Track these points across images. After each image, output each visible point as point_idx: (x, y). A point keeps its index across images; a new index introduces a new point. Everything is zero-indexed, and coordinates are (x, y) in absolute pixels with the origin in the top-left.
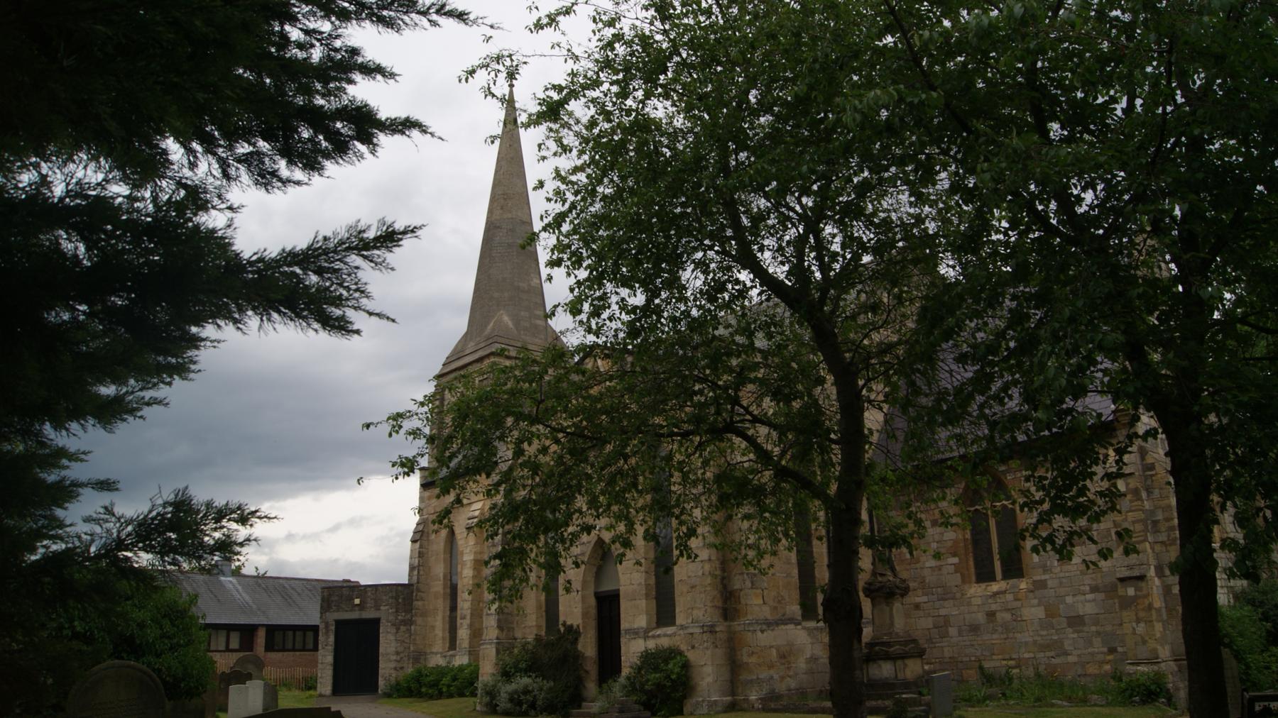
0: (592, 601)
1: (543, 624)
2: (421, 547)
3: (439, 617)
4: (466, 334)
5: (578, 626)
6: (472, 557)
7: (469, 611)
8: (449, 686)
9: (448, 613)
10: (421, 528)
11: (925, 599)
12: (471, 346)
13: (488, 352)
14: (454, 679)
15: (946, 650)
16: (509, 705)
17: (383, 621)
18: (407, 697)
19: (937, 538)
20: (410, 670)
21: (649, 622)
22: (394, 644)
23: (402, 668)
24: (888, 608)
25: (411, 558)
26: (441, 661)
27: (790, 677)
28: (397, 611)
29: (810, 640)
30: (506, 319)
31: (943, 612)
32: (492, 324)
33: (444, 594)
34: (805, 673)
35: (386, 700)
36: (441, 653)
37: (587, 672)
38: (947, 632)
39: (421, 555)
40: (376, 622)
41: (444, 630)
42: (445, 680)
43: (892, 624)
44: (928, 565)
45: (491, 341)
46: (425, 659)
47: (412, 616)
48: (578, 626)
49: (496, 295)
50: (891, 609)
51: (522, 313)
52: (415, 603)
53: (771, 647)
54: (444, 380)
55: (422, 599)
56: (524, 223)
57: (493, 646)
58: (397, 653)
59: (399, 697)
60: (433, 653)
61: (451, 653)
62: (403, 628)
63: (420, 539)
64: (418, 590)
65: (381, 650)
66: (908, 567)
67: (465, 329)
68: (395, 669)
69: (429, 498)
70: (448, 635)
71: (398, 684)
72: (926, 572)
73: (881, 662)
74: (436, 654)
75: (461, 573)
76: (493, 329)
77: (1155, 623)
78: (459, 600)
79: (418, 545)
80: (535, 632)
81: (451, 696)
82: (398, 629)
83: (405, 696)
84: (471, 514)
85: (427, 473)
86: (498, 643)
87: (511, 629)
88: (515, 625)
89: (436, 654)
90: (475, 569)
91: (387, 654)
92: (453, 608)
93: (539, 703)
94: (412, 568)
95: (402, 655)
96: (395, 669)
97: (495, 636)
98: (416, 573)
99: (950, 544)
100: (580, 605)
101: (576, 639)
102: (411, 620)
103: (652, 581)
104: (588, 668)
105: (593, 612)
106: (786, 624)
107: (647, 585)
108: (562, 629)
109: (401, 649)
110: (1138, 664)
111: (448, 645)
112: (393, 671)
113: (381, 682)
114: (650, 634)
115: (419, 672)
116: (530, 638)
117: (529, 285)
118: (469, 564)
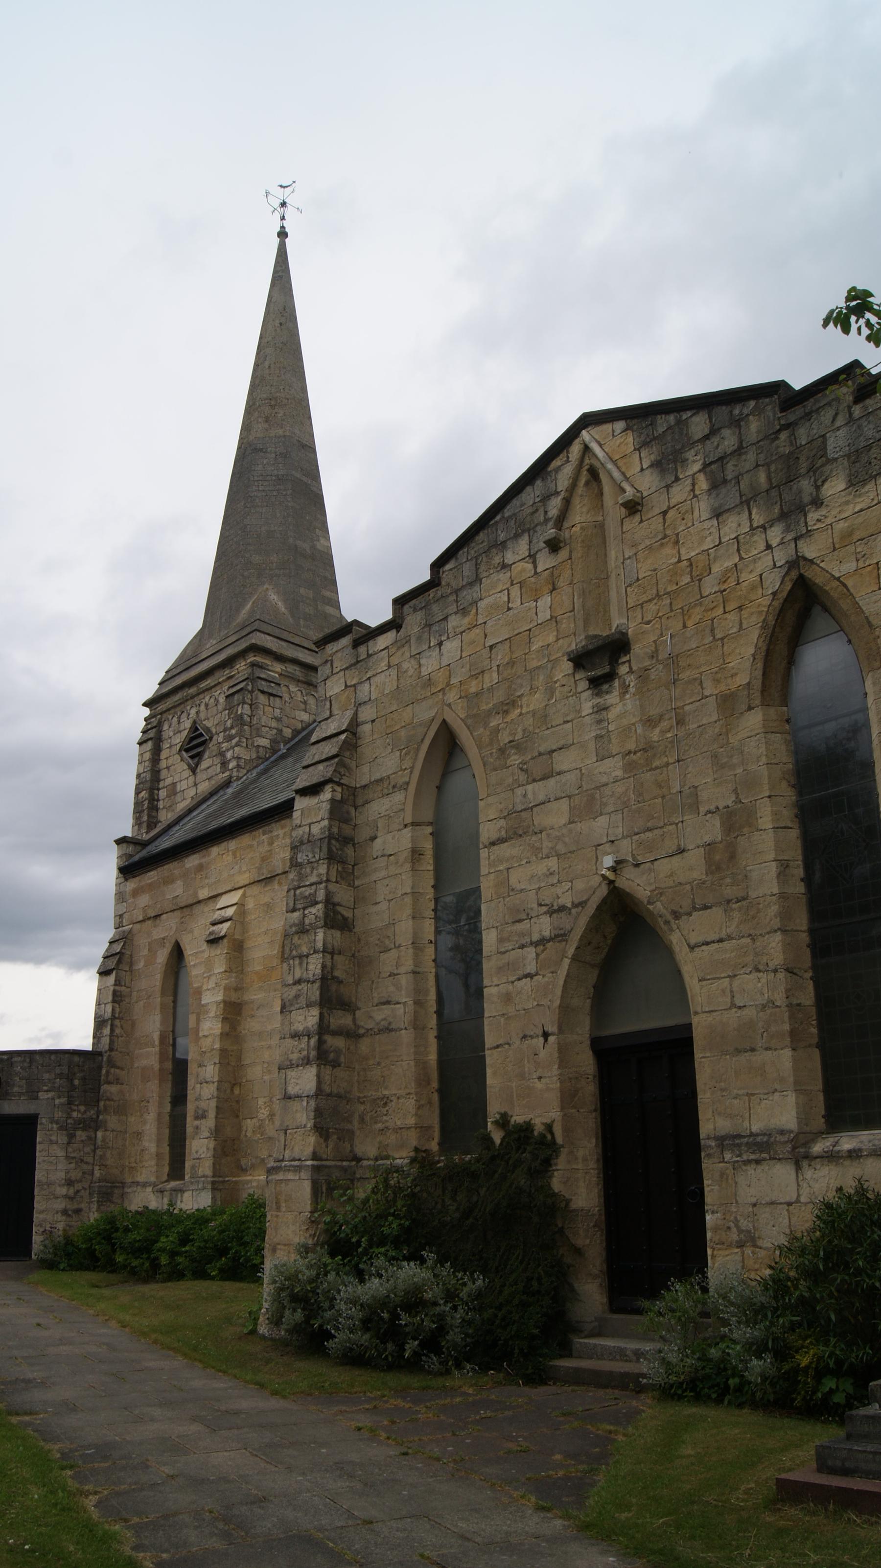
0: (586, 1062)
1: (435, 1122)
2: (118, 983)
3: (151, 1117)
4: (201, 629)
5: (549, 1127)
6: (220, 997)
7: (213, 1104)
8: (173, 1254)
9: (168, 1108)
10: (117, 948)
12: (211, 645)
13: (242, 645)
14: (184, 1240)
16: (365, 1338)
17: (43, 1121)
18: (87, 1269)
20: (93, 1216)
21: (804, 1117)
22: (62, 1165)
23: (78, 1211)
25: (98, 1004)
26: (151, 1200)
28: (70, 1103)
30: (273, 597)
32: (248, 606)
33: (161, 1070)
35: (45, 1274)
36: (154, 1185)
37: (578, 1252)
39: (117, 998)
40: (30, 1122)
41: (159, 1141)
42: (165, 1242)
45: (248, 629)
46: (123, 1196)
47: (98, 1113)
48: (549, 1127)
49: (256, 559)
51: (302, 591)
52: (105, 1087)
54: (162, 707)
55: (118, 1081)
56: (304, 446)
57: (305, 1175)
58: (69, 1183)
59: (72, 1268)
60: (138, 1184)
61: (173, 1184)
62: (81, 1135)
63: (117, 968)
64: (111, 1064)
65: (39, 1175)
67: (199, 625)
68: (65, 1212)
69: (135, 893)
70: (167, 1149)
71: (68, 1241)
74: (145, 1185)
75: (197, 1030)
76: (252, 611)
78: (191, 1081)
79: (112, 979)
80: (414, 1143)
81: (176, 1275)
82: (71, 1137)
83: (80, 1267)
84: (217, 915)
85: (131, 849)
86: (316, 1169)
87: (347, 1135)
88: (356, 1124)
89: (145, 1185)
90: (225, 1019)
91: (49, 1184)
92: (179, 1098)
93: (454, 1336)
94: (99, 1023)
95: (78, 1186)
96: (65, 1212)
97: (309, 1151)
98: (107, 1031)
100: (555, 1070)
101: (547, 1163)
102: (96, 1120)
103: (807, 997)
104: (581, 1241)
105: (590, 1089)
107: (794, 1008)
108: (497, 1137)
109: (75, 1175)
110: (342, 1160)
111: (166, 1169)
112: (59, 1217)
113: (37, 1239)
114: (818, 1148)
115: (111, 1221)
116: (401, 1158)
117: (313, 547)
118: (213, 1011)
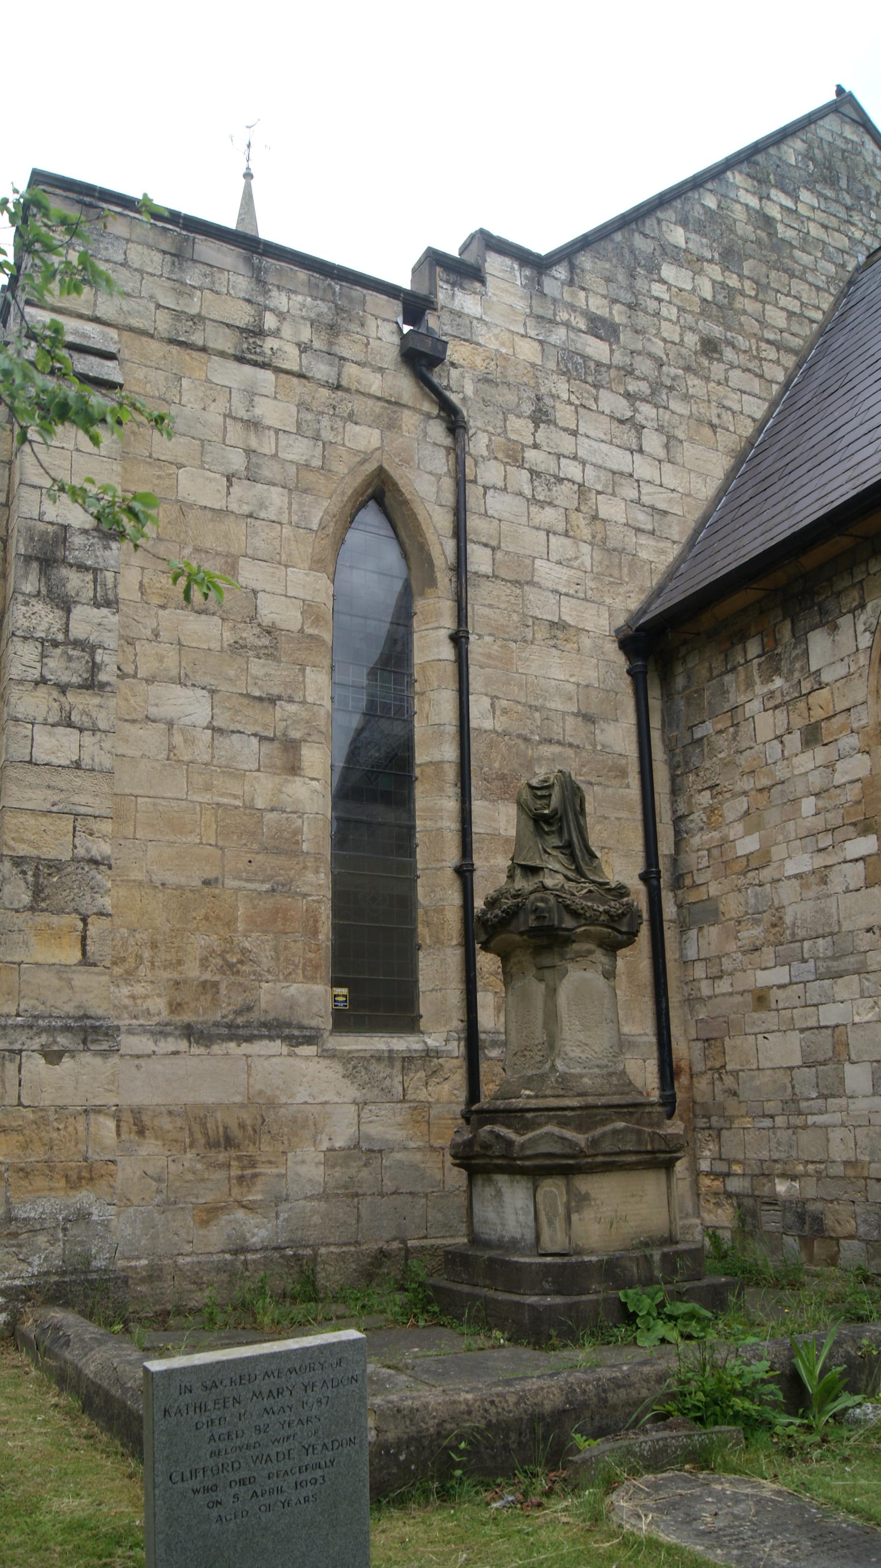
11: (780, 975)
15: (836, 1135)
19: (816, 780)
24: (538, 989)
27: (249, 1207)
29: (351, 1092)
31: (830, 1015)
34: (324, 1196)
38: (842, 1080)
43: (551, 1044)
44: (791, 868)
50: (552, 992)
53: (98, 1110)
66: (741, 881)
72: (787, 892)
73: (502, 1180)
77: (756, 835)
99: (853, 793)
106: (249, 1039)
